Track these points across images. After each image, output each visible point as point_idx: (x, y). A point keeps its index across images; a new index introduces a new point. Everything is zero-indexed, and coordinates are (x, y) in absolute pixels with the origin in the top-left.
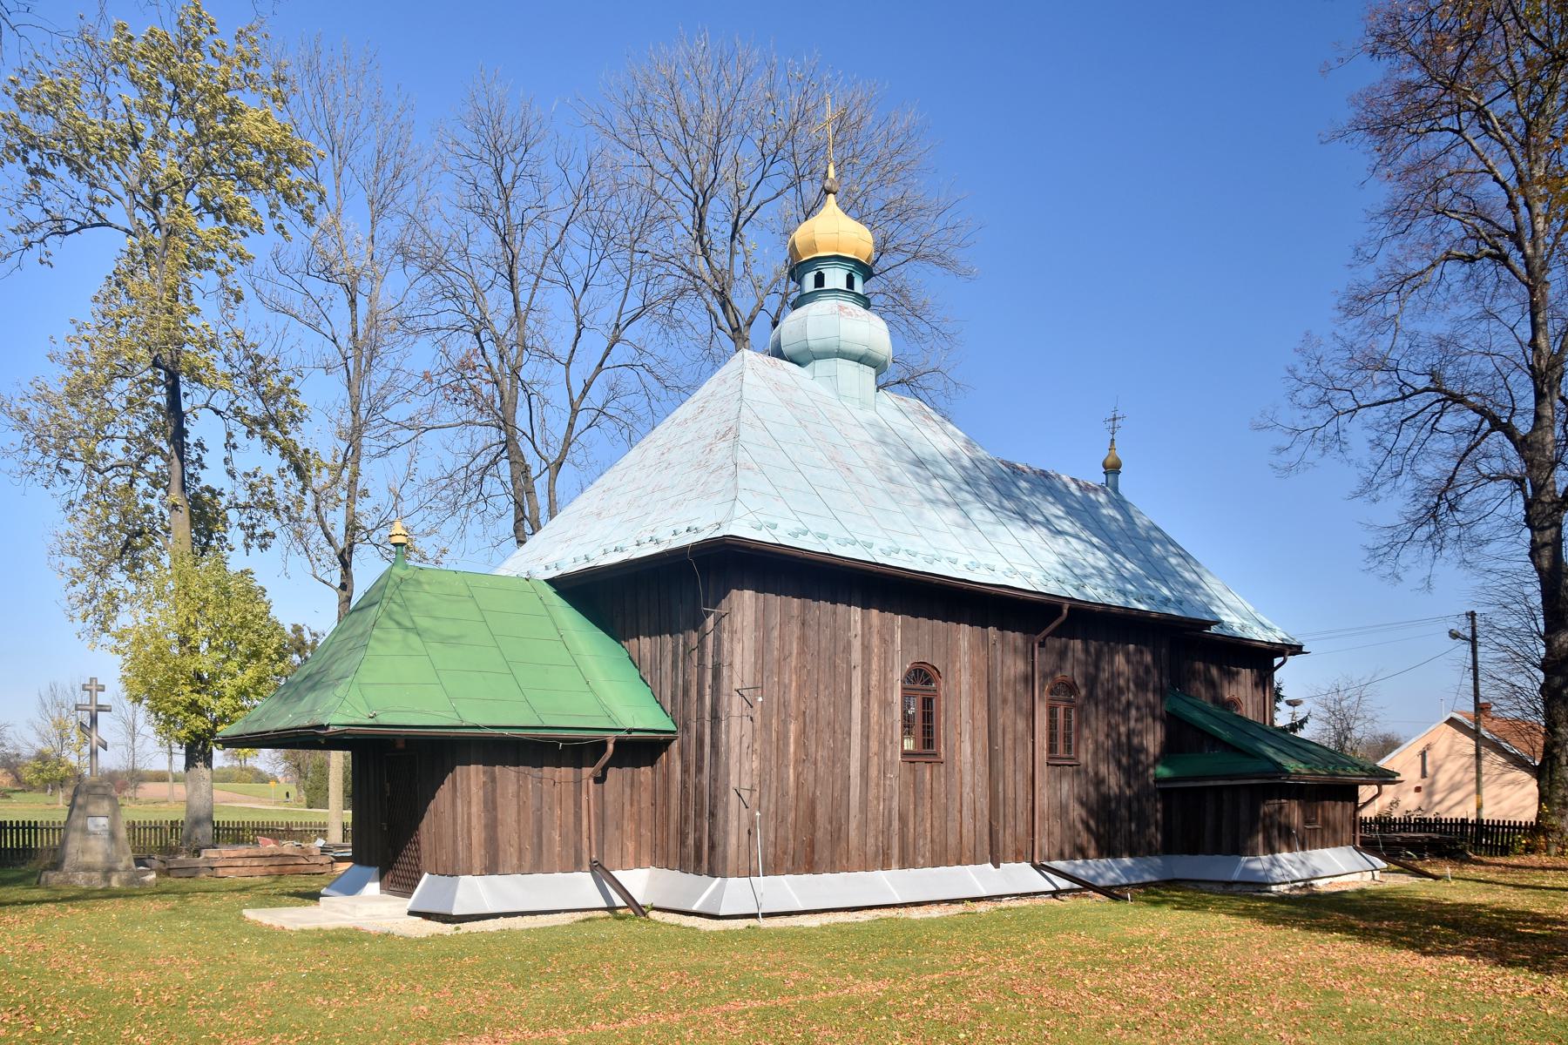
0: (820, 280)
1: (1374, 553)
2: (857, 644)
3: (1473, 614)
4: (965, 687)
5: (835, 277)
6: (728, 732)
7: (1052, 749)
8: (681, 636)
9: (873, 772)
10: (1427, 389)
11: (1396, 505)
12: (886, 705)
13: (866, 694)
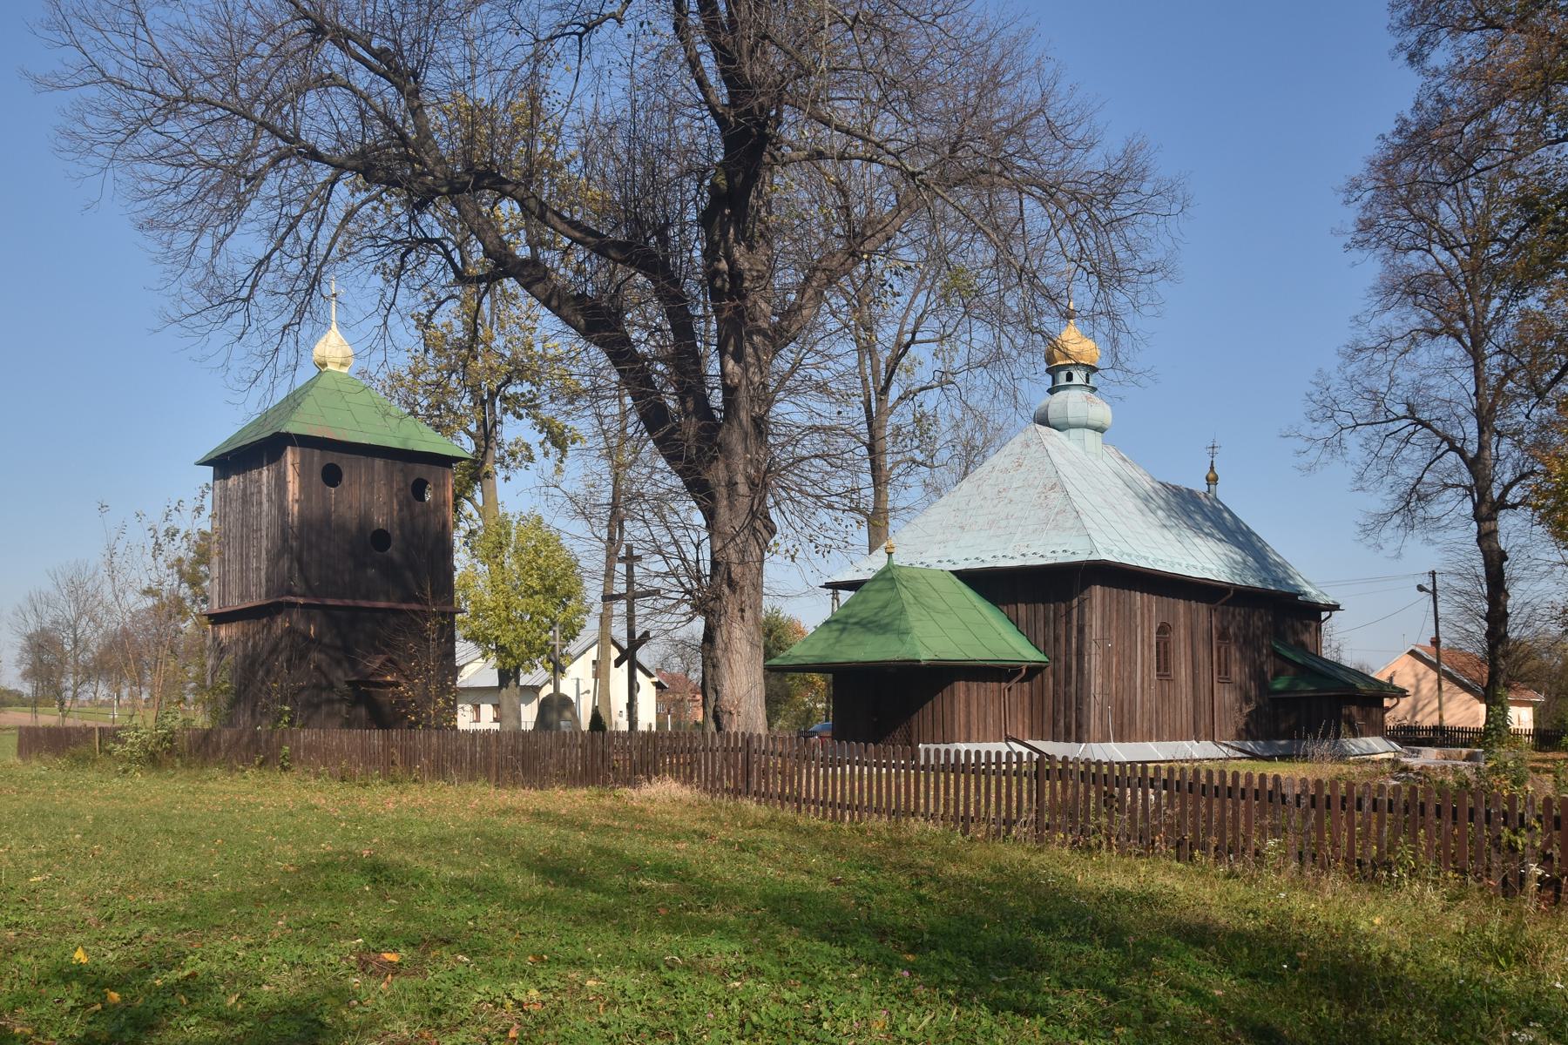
0: (1070, 377)
1: (1365, 530)
2: (1139, 613)
3: (1433, 573)
4: (1182, 637)
5: (1078, 377)
6: (1090, 663)
7: (1219, 673)
8: (1042, 606)
9: (1146, 686)
10: (1405, 417)
11: (1381, 499)
12: (1150, 646)
13: (1143, 640)
